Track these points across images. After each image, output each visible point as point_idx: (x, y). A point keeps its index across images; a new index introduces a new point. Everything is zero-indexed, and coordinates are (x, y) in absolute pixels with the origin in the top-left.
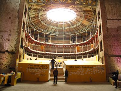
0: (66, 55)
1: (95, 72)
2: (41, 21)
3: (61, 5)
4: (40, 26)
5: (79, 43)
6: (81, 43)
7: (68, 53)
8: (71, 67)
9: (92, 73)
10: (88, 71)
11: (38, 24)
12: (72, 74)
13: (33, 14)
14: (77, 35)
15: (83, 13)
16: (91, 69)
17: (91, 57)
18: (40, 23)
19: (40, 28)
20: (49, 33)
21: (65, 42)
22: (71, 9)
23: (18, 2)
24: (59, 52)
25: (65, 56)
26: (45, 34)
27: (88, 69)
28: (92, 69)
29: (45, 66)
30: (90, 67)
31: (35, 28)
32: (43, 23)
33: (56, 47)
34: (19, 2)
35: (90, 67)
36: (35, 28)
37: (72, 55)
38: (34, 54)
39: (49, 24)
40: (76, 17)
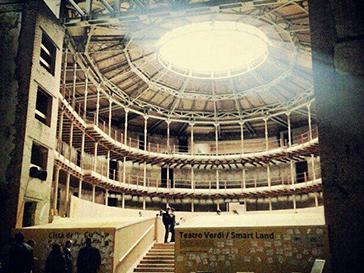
0: (254, 196)
1: (283, 256)
2: (145, 79)
3: (173, 14)
4: (147, 95)
5: (300, 147)
6: (307, 144)
7: (261, 190)
8: (190, 236)
9: (270, 260)
10: (253, 251)
11: (137, 89)
12: (194, 261)
13: (107, 55)
14: (269, 120)
15: (284, 25)
16: (268, 244)
17: (295, 210)
18: (141, 85)
19: (149, 105)
20: (187, 119)
21: (272, 146)
22: (237, 21)
23: (16, 26)
24: (253, 186)
25: (252, 201)
26: (168, 122)
27: (255, 243)
28: (273, 245)
29: (200, 235)
30: (262, 236)
31: (127, 104)
32: (152, 85)
33: (189, 166)
34: (20, 25)
35: (262, 236)
36: (127, 104)
37: (199, 197)
38: (113, 196)
39: (177, 85)
40: (269, 47)
